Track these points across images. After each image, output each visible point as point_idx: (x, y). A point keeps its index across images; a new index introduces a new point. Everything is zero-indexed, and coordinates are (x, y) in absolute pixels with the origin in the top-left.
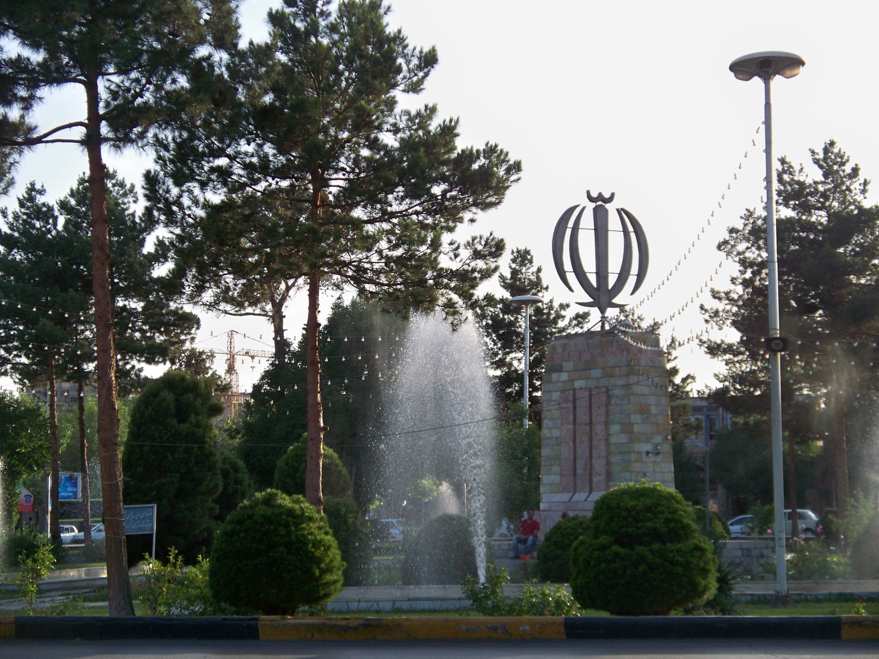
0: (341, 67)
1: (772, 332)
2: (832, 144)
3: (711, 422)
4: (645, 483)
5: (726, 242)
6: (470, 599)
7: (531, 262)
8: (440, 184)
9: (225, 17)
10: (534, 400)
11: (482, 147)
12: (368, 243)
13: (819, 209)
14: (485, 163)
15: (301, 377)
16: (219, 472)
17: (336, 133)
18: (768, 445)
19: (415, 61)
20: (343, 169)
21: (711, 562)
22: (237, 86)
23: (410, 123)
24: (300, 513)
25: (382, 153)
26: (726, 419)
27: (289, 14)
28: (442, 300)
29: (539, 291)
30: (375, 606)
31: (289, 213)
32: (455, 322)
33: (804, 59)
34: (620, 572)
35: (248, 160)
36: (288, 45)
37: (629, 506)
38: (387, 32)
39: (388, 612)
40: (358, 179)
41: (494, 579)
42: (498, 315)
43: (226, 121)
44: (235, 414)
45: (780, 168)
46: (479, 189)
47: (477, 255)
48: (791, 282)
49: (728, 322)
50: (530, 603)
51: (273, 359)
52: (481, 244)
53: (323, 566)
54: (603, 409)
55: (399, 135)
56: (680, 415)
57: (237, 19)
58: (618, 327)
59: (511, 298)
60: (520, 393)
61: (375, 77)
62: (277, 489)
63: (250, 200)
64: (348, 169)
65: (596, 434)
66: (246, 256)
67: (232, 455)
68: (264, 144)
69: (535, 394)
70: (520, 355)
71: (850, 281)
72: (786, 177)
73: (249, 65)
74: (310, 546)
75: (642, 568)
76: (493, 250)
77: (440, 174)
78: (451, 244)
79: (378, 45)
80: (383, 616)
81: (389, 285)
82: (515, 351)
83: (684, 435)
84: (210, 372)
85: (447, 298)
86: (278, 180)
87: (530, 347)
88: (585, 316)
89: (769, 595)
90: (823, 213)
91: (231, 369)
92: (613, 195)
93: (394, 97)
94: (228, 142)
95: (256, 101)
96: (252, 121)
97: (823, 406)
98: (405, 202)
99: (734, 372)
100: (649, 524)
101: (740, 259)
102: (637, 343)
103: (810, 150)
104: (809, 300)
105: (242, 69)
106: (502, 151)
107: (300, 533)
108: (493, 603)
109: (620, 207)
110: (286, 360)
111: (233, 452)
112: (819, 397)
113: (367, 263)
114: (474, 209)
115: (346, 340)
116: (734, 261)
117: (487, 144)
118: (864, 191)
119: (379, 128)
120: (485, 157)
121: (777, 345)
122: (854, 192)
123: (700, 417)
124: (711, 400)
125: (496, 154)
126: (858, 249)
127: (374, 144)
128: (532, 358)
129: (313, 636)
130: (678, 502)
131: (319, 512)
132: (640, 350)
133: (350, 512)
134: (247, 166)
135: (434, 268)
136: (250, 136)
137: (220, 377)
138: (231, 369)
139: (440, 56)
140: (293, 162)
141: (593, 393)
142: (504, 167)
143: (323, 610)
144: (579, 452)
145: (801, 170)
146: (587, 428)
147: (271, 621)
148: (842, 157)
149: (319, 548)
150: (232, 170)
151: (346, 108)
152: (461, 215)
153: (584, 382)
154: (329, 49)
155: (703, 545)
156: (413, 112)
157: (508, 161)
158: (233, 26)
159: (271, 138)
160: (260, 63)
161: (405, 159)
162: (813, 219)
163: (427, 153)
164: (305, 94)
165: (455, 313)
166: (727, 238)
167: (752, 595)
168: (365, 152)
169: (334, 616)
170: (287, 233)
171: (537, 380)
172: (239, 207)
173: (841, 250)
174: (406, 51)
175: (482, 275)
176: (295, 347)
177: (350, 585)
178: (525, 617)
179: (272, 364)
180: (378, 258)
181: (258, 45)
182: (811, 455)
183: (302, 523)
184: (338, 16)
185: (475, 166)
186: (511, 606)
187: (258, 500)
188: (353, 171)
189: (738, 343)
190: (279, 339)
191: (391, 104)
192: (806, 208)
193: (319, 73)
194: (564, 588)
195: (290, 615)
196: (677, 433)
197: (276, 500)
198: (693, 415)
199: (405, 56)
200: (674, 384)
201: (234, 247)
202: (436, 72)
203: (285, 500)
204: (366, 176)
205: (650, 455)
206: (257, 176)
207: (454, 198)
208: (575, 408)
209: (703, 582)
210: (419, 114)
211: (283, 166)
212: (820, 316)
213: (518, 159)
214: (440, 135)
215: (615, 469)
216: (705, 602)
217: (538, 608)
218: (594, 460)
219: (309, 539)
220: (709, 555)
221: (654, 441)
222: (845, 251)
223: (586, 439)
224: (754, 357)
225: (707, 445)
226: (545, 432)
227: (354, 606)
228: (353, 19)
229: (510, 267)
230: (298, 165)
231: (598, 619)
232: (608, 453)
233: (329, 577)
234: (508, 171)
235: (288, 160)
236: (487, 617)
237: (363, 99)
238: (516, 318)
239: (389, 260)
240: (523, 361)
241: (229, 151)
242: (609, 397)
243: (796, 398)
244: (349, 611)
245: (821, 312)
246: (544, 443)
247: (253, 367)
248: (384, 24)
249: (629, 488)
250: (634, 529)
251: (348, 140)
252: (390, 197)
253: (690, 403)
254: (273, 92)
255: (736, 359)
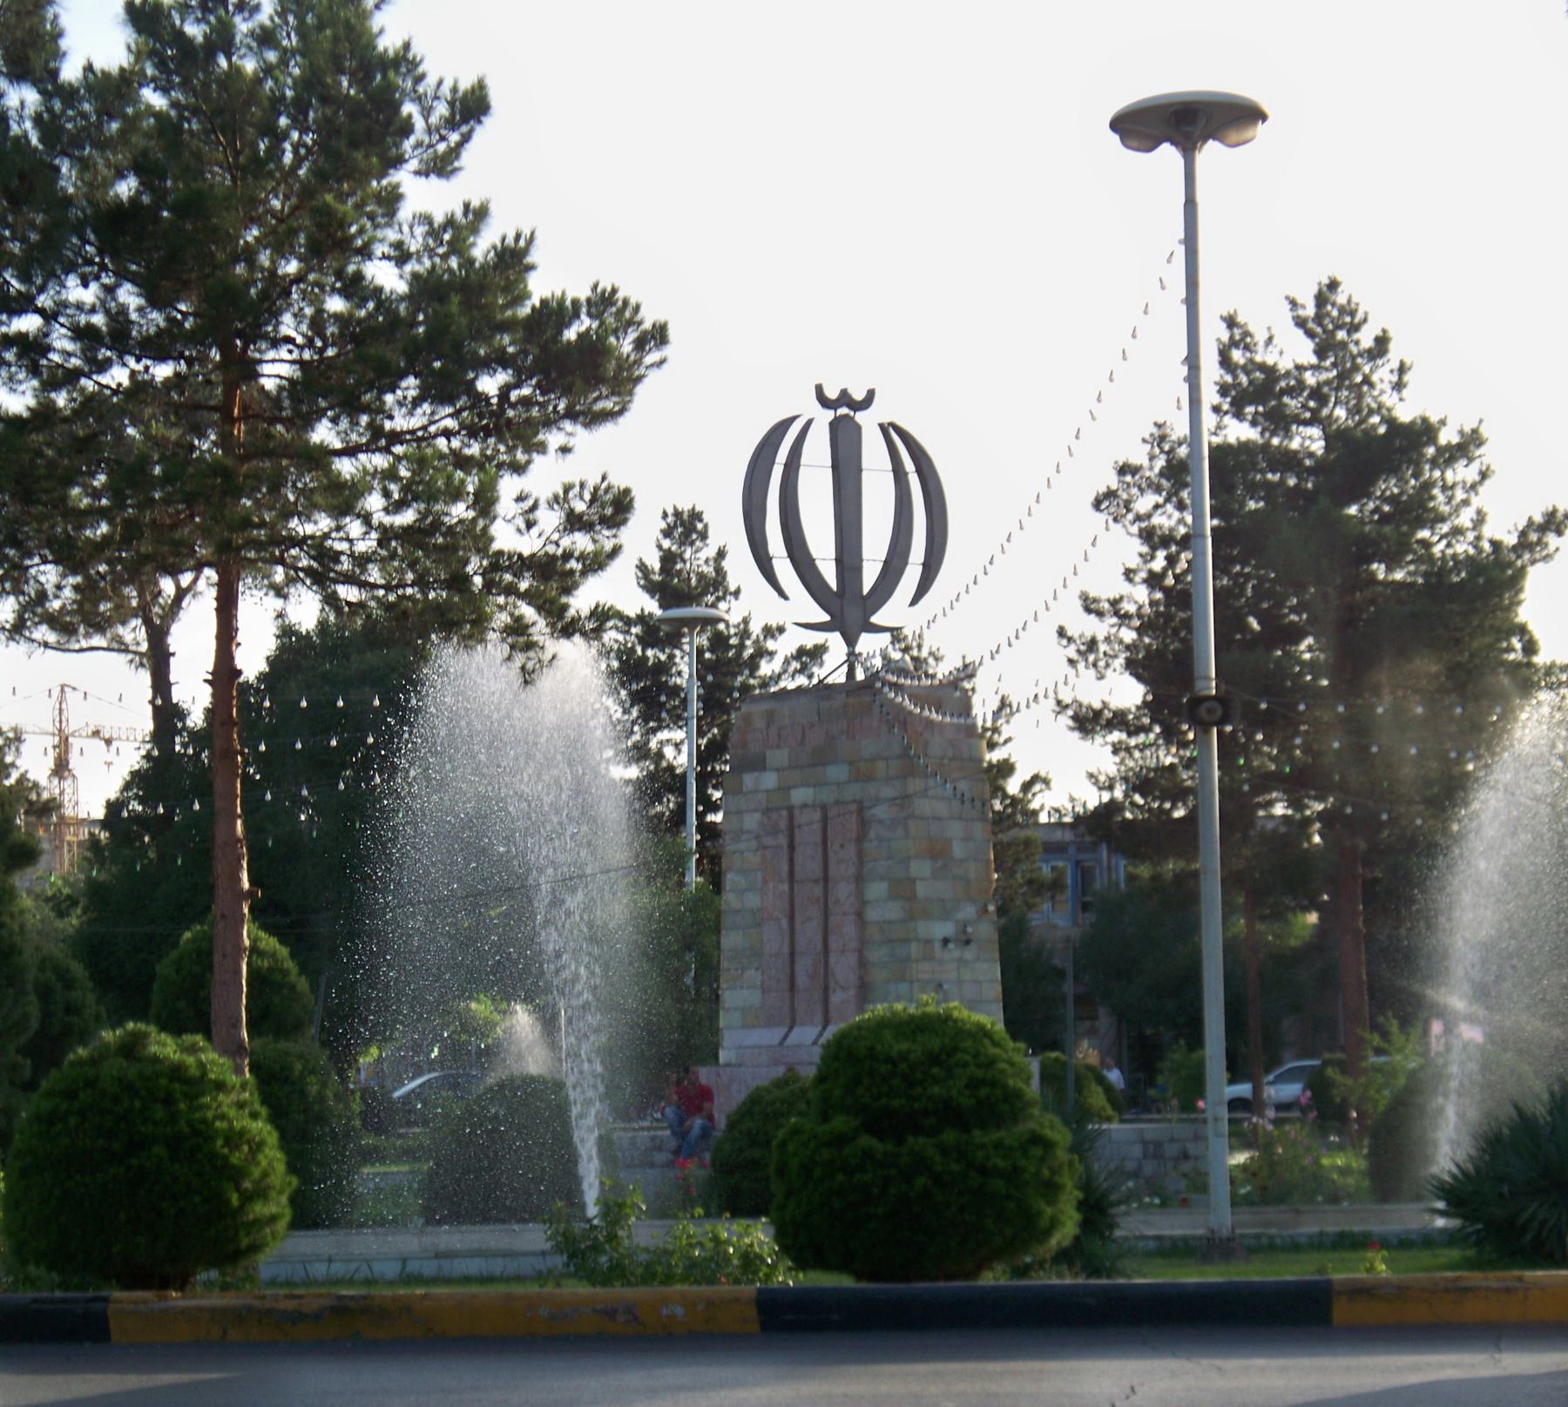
0: (283, 121)
1: (1199, 685)
2: (1333, 285)
3: (1085, 876)
4: (927, 1004)
5: (1110, 494)
6: (562, 1253)
7: (704, 536)
8: (495, 371)
9: (29, 13)
10: (708, 831)
11: (583, 293)
12: (343, 500)
13: (1306, 423)
14: (589, 329)
15: (203, 785)
16: (30, 987)
17: (273, 262)
18: (1190, 928)
19: (442, 110)
20: (289, 340)
21: (1066, 1169)
22: (57, 161)
23: (431, 241)
24: (198, 1074)
25: (371, 305)
26: (1115, 870)
27: (170, 8)
28: (503, 619)
29: (718, 599)
30: (364, 1271)
31: (174, 434)
32: (530, 665)
33: (1266, 107)
34: (875, 1191)
35: (83, 319)
36: (169, 73)
37: (894, 1053)
38: (381, 48)
39: (391, 1283)
40: (322, 360)
41: (614, 1210)
42: (633, 649)
43: (34, 237)
44: (72, 865)
45: (1225, 337)
46: (579, 383)
47: (574, 522)
48: (1248, 577)
49: (1119, 662)
50: (690, 1258)
51: (149, 746)
52: (582, 498)
53: (247, 1185)
54: (851, 850)
55: (408, 268)
56: (1017, 861)
57: (56, 17)
58: (882, 674)
59: (658, 612)
60: (679, 817)
61: (354, 144)
62: (148, 1023)
63: (92, 405)
64: (300, 340)
65: (837, 902)
66: (80, 527)
67: (58, 951)
68: (117, 286)
69: (710, 818)
70: (679, 735)
71: (1373, 574)
72: (1237, 356)
73: (84, 115)
74: (220, 1142)
75: (921, 1181)
76: (609, 511)
77: (495, 351)
78: (520, 499)
79: (361, 75)
80: (375, 1291)
81: (388, 588)
82: (668, 726)
83: (1026, 903)
84: (15, 776)
85: (512, 615)
86: (149, 362)
87: (699, 719)
88: (817, 653)
89: (1194, 1237)
90: (1315, 432)
91: (61, 768)
92: (871, 394)
93: (397, 186)
94: (39, 281)
95: (98, 195)
96: (92, 237)
97: (1317, 839)
98: (419, 411)
99: (1131, 769)
100: (936, 1090)
101: (1141, 530)
102: (922, 709)
103: (1287, 298)
104: (1287, 615)
105: (69, 126)
106: (626, 302)
107: (197, 1115)
108: (611, 1260)
109: (886, 420)
110: (178, 748)
111: (61, 945)
112: (1307, 822)
113: (341, 539)
114: (568, 425)
115: (304, 704)
116: (1129, 533)
117: (595, 286)
118: (1399, 386)
119: (366, 253)
120: (589, 315)
121: (1210, 711)
122: (1379, 386)
123: (1060, 864)
124: (1082, 829)
125: (614, 309)
126: (1387, 508)
127: (354, 287)
128: (704, 742)
129: (225, 1333)
130: (995, 1044)
131: (238, 1070)
132: (930, 723)
133: (312, 1072)
134: (84, 334)
135: (482, 550)
136: (88, 269)
137: (36, 785)
138: (61, 768)
139: (495, 97)
140: (180, 324)
141: (830, 814)
142: (632, 335)
143: (251, 1279)
144: (802, 942)
145: (1270, 340)
146: (818, 891)
147: (135, 1302)
148: (1353, 313)
149: (238, 1147)
150: (48, 340)
151: (294, 209)
152: (541, 437)
153: (810, 791)
154: (258, 81)
155: (1048, 1132)
156: (439, 219)
157: (640, 323)
158: (46, 33)
159: (134, 273)
160: (106, 112)
161: (421, 317)
162: (1295, 444)
163: (467, 306)
164: (205, 180)
165: (530, 646)
166: (1114, 487)
167: (1159, 1238)
168: (335, 304)
169: (269, 1292)
170: (166, 479)
171: (715, 787)
172: (66, 420)
173: (1353, 510)
174: (421, 89)
175: (584, 564)
176: (196, 719)
177: (307, 1227)
178: (678, 1287)
179: (148, 757)
180: (364, 529)
181: (103, 72)
182: (1293, 942)
183: (203, 1094)
184: (277, 12)
185: (571, 334)
186: (648, 1266)
187: (107, 1046)
188: (310, 343)
189: (1138, 708)
190: (159, 702)
191: (391, 200)
192: (1279, 421)
193: (234, 133)
194: (760, 1226)
195: (176, 1290)
196: (1012, 900)
197: (144, 1046)
198: (1047, 862)
199: (419, 98)
200: (1005, 795)
201: (55, 507)
202: (485, 134)
203: (165, 1046)
204: (338, 355)
205: (951, 946)
206: (104, 353)
207: (526, 402)
208: (792, 847)
209: (1049, 1211)
210: (450, 222)
211: (160, 332)
212: (1310, 649)
213: (662, 319)
214: (496, 266)
215: (878, 975)
216: (1053, 1253)
217: (707, 1268)
218: (832, 959)
219: (217, 1131)
220: (1062, 1155)
221: (961, 915)
222: (1361, 511)
223: (815, 911)
224: (1171, 735)
225: (1075, 923)
226: (729, 899)
227: (319, 1270)
228: (309, 19)
229: (660, 547)
230: (192, 331)
231: (835, 1290)
232: (863, 943)
233: (259, 1209)
234: (640, 344)
235: (171, 320)
236: (598, 1290)
237: (330, 191)
238: (671, 657)
239: (386, 534)
240: (685, 748)
241: (43, 301)
242: (864, 824)
243: (1260, 823)
244: (309, 1282)
245: (1309, 640)
246: (726, 921)
247: (109, 764)
248: (375, 29)
249: (895, 1014)
250: (904, 1101)
251: (299, 278)
252: (389, 398)
253: (1038, 835)
254: (136, 174)
255: (1133, 742)
